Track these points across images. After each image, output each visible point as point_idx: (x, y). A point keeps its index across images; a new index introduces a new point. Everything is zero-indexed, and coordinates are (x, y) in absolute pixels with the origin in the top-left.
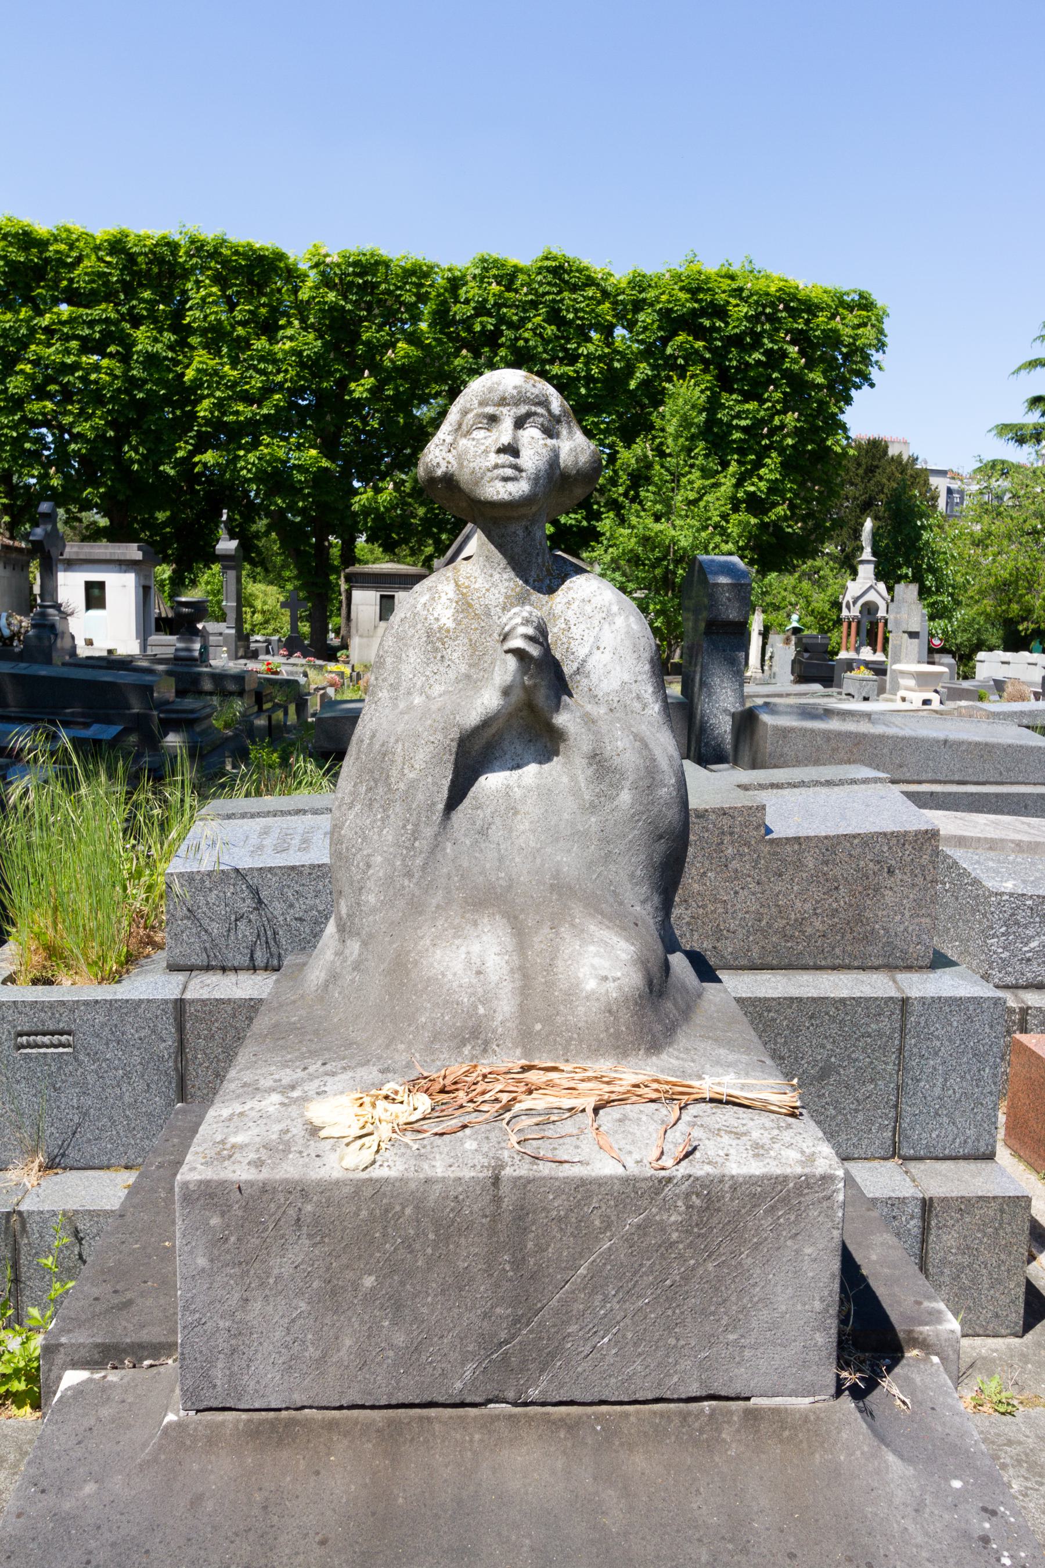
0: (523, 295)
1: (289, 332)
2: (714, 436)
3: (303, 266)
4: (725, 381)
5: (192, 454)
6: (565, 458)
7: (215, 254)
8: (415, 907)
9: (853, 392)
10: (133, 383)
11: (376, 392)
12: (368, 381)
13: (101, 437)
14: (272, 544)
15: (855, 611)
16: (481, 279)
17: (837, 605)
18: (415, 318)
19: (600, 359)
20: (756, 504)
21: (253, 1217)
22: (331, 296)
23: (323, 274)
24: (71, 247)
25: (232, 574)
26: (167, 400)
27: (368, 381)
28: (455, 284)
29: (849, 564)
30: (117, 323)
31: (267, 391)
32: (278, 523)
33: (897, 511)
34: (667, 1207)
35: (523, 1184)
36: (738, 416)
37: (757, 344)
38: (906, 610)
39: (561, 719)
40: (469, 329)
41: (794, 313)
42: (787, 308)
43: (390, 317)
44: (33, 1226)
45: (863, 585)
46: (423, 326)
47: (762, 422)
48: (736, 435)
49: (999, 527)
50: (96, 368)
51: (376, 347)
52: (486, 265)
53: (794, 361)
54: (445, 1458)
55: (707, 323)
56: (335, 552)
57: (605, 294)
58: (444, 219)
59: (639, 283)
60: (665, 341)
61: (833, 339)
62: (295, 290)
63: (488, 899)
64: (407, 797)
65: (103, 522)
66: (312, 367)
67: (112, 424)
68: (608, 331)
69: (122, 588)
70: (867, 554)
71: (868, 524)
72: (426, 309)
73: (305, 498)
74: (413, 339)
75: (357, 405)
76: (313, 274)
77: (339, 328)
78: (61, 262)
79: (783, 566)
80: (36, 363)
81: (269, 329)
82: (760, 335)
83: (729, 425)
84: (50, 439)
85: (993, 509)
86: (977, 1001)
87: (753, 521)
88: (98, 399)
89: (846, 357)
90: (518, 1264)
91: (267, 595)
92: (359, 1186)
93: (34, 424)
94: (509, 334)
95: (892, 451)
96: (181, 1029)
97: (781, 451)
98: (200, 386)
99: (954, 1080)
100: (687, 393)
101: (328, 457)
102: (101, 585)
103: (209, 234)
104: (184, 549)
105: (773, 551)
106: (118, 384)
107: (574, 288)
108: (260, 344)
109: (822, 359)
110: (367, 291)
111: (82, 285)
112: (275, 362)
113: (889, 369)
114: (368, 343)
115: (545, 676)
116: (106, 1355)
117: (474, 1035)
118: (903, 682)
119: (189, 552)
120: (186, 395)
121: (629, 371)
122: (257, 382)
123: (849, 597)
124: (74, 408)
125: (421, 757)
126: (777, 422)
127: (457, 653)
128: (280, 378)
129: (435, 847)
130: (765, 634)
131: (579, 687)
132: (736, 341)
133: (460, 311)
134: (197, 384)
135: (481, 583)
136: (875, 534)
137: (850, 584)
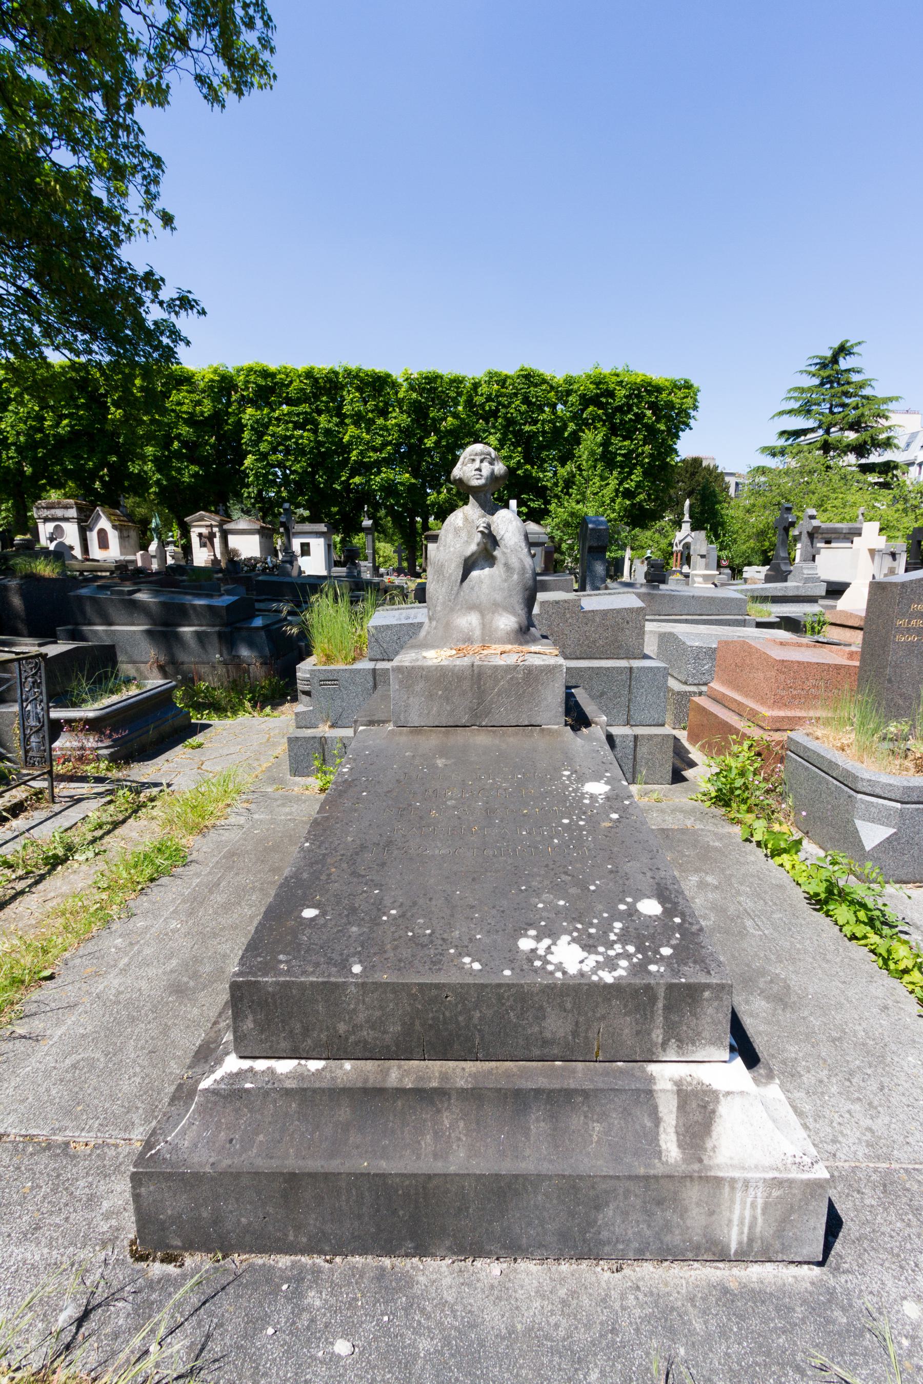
0: (510, 390)
1: (394, 415)
2: (607, 459)
3: (400, 380)
4: (614, 430)
5: (349, 478)
6: (496, 472)
7: (357, 376)
8: (452, 610)
9: (681, 433)
10: (320, 444)
11: (437, 443)
12: (433, 438)
13: (305, 471)
14: (388, 522)
15: (680, 548)
16: (488, 383)
17: (671, 545)
18: (457, 404)
19: (549, 421)
20: (628, 494)
21: (410, 675)
22: (414, 395)
23: (410, 384)
24: (287, 376)
25: (370, 537)
26: (335, 452)
27: (433, 438)
28: (476, 386)
29: (678, 524)
30: (310, 414)
31: (385, 444)
32: (390, 511)
33: (705, 497)
34: (518, 673)
35: (481, 666)
36: (620, 449)
37: (630, 409)
38: (699, 542)
39: (496, 553)
40: (483, 409)
41: (649, 393)
42: (646, 390)
43: (444, 405)
44: (329, 742)
45: (684, 533)
46: (460, 408)
47: (632, 451)
48: (619, 458)
49: (761, 501)
50: (302, 437)
51: (435, 415)
52: (491, 375)
53: (649, 418)
54: (460, 737)
55: (604, 400)
56: (419, 526)
57: (552, 387)
58: (472, 351)
59: (569, 381)
60: (583, 411)
61: (670, 405)
62: (397, 393)
63: (473, 607)
64: (449, 578)
65: (306, 513)
66: (406, 432)
67: (309, 465)
68: (554, 406)
69: (318, 545)
70: (686, 518)
71: (687, 502)
72: (462, 400)
73: (404, 498)
74: (456, 416)
75: (429, 450)
76: (405, 384)
77: (418, 411)
78: (283, 384)
79: (644, 527)
80: (272, 436)
81: (384, 413)
82: (632, 405)
83: (616, 454)
84: (279, 473)
85: (756, 492)
86: (658, 668)
87: (628, 502)
88: (303, 453)
89: (677, 414)
90: (479, 688)
91: (386, 549)
92: (437, 667)
93: (273, 466)
94: (503, 411)
95: (704, 464)
96: (375, 679)
97: (642, 466)
98: (352, 444)
99: (649, 697)
100: (591, 439)
101: (415, 478)
102: (308, 544)
103: (353, 366)
104: (347, 525)
105: (640, 517)
106: (312, 444)
107: (536, 385)
108: (380, 421)
109: (664, 416)
110: (433, 391)
111: (293, 395)
112: (387, 430)
113: (700, 421)
114: (433, 419)
115: (490, 540)
116: (371, 723)
117: (469, 640)
118: (696, 579)
119: (347, 525)
120: (345, 449)
121: (565, 426)
122: (379, 441)
123: (677, 540)
124: (292, 458)
125: (453, 566)
126: (640, 450)
127: (464, 534)
128: (390, 438)
129: (458, 593)
130: (631, 561)
131: (502, 543)
132: (619, 409)
133: (478, 400)
134: (350, 443)
135: (471, 512)
136: (691, 506)
137: (678, 533)
